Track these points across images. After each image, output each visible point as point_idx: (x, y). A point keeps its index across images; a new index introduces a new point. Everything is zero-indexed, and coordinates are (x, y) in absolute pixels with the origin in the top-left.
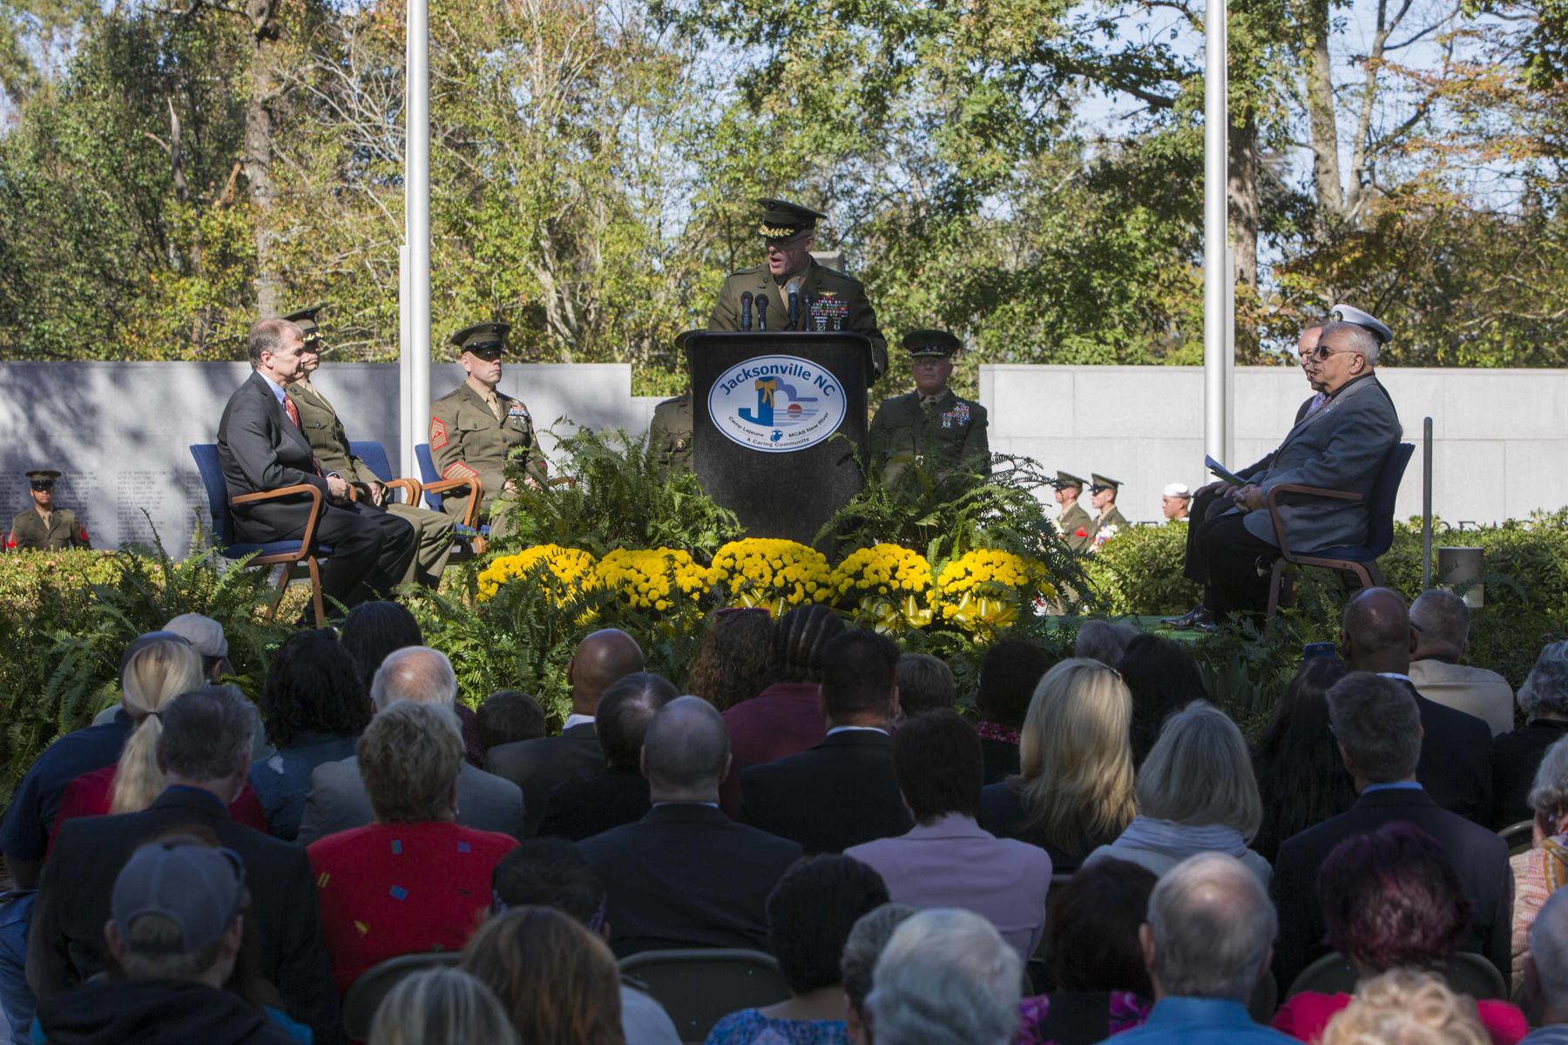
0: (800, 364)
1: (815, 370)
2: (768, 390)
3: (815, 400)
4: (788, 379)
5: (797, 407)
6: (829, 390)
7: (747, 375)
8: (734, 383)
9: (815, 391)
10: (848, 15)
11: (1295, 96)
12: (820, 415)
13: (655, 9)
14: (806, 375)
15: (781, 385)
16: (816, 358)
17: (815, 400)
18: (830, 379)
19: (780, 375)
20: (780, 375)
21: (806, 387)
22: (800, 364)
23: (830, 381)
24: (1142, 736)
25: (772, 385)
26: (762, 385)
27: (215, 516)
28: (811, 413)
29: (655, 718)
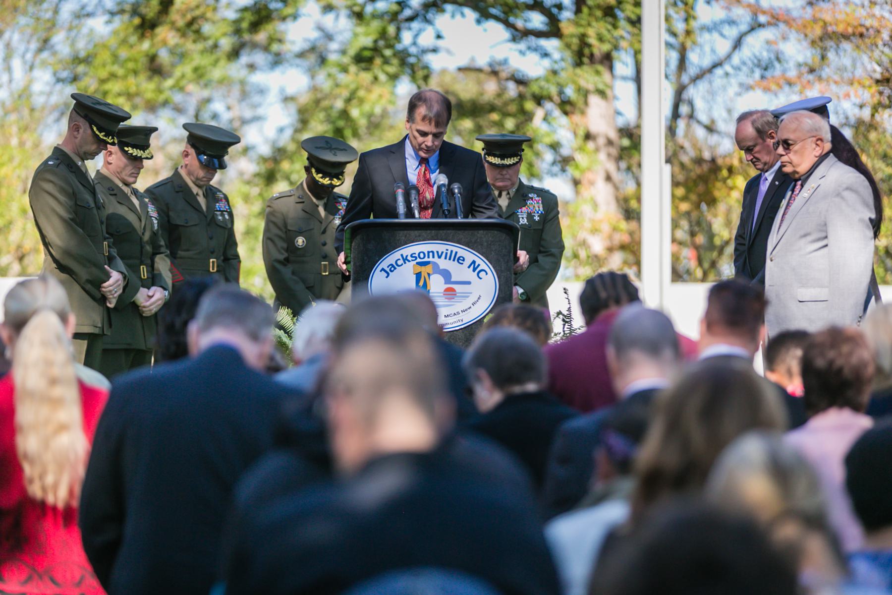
0: (455, 249)
1: (470, 256)
2: (424, 274)
3: (469, 283)
4: (443, 264)
5: (453, 290)
6: (482, 274)
7: (405, 260)
8: (393, 267)
9: (470, 275)
10: (873, 3)
11: (738, 44)
12: (473, 298)
13: (871, 2)
14: (460, 260)
15: (437, 270)
16: (470, 244)
17: (469, 283)
18: (483, 264)
19: (436, 259)
20: (436, 259)
21: (460, 272)
22: (455, 249)
23: (483, 266)
24: (782, 390)
25: (429, 269)
26: (419, 269)
27: (237, 257)
28: (466, 296)
29: (606, 259)
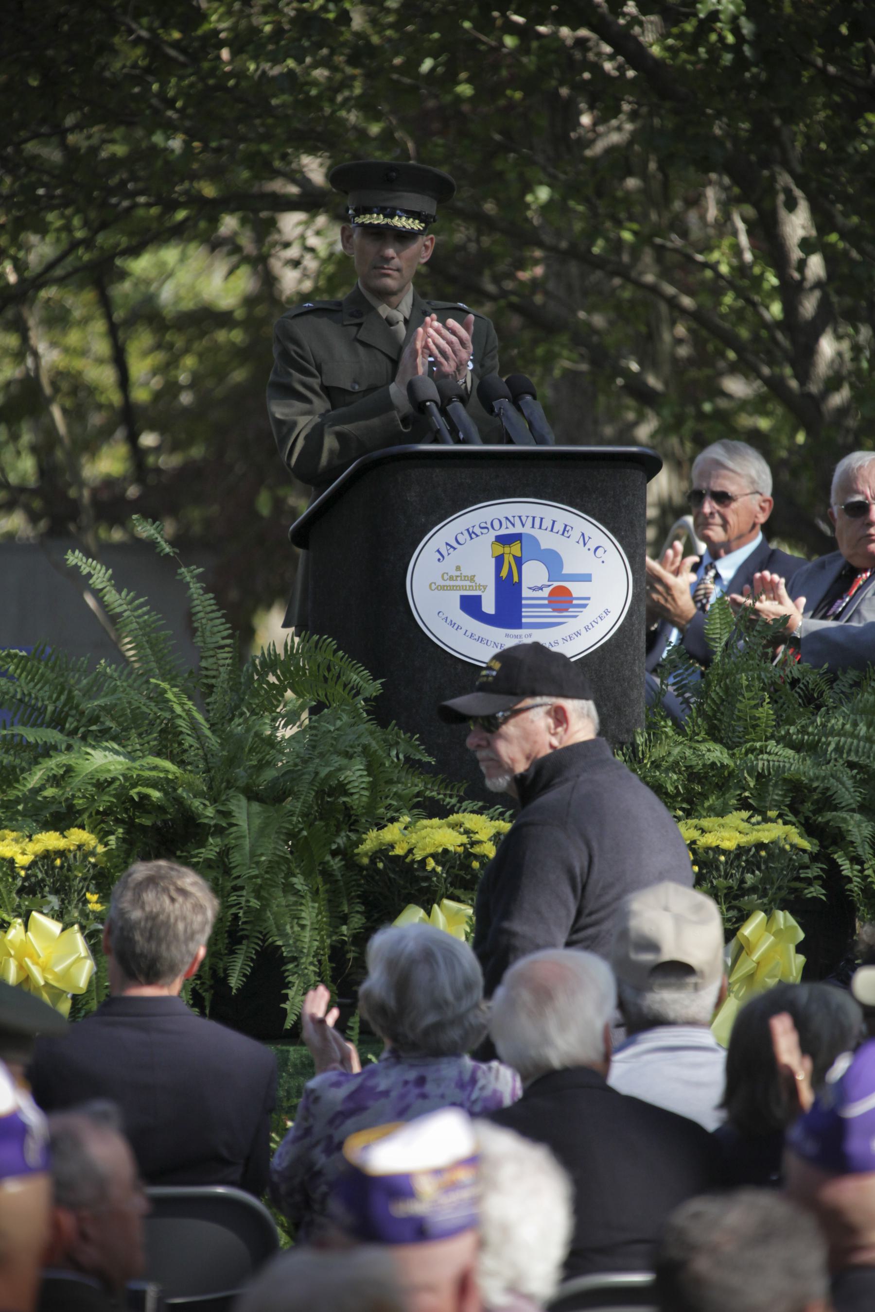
2: (508, 559)
